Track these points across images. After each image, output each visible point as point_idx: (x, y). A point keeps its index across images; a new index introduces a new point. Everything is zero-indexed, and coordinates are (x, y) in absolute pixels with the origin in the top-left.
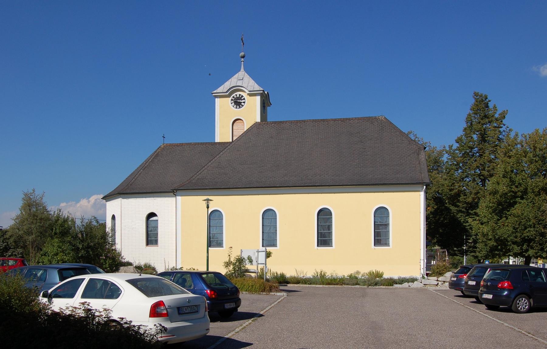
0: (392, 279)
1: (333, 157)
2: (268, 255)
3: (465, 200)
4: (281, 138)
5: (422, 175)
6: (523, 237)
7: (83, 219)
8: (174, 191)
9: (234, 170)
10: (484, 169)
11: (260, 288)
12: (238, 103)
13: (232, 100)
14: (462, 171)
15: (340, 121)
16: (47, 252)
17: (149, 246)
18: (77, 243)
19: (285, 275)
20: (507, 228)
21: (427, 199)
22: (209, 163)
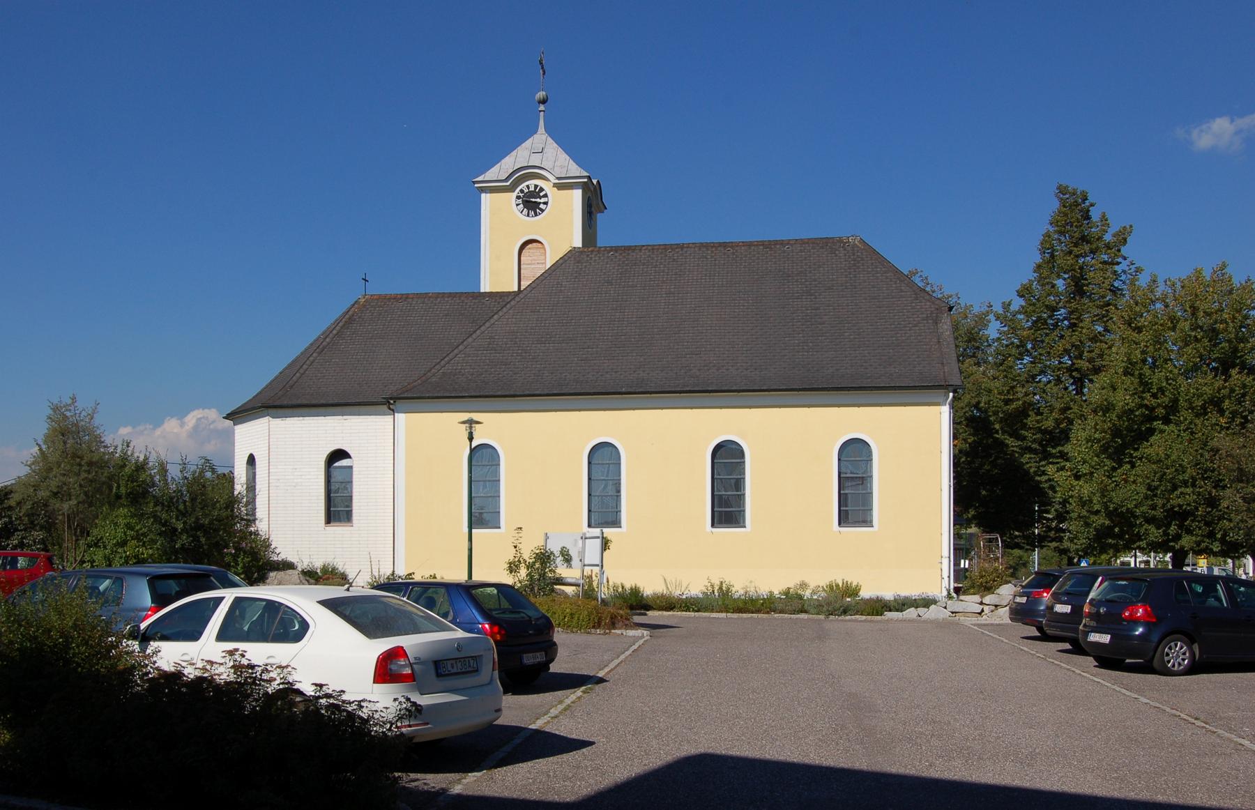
1: (746, 328)
2: (605, 544)
6: (1169, 507)
7: (185, 464)
8: (389, 402)
9: (524, 354)
10: (1080, 357)
11: (590, 620)
12: (532, 203)
13: (518, 197)
15: (761, 247)
16: (102, 538)
17: (332, 524)
18: (171, 518)
19: (642, 590)
20: (1133, 487)
21: (956, 423)
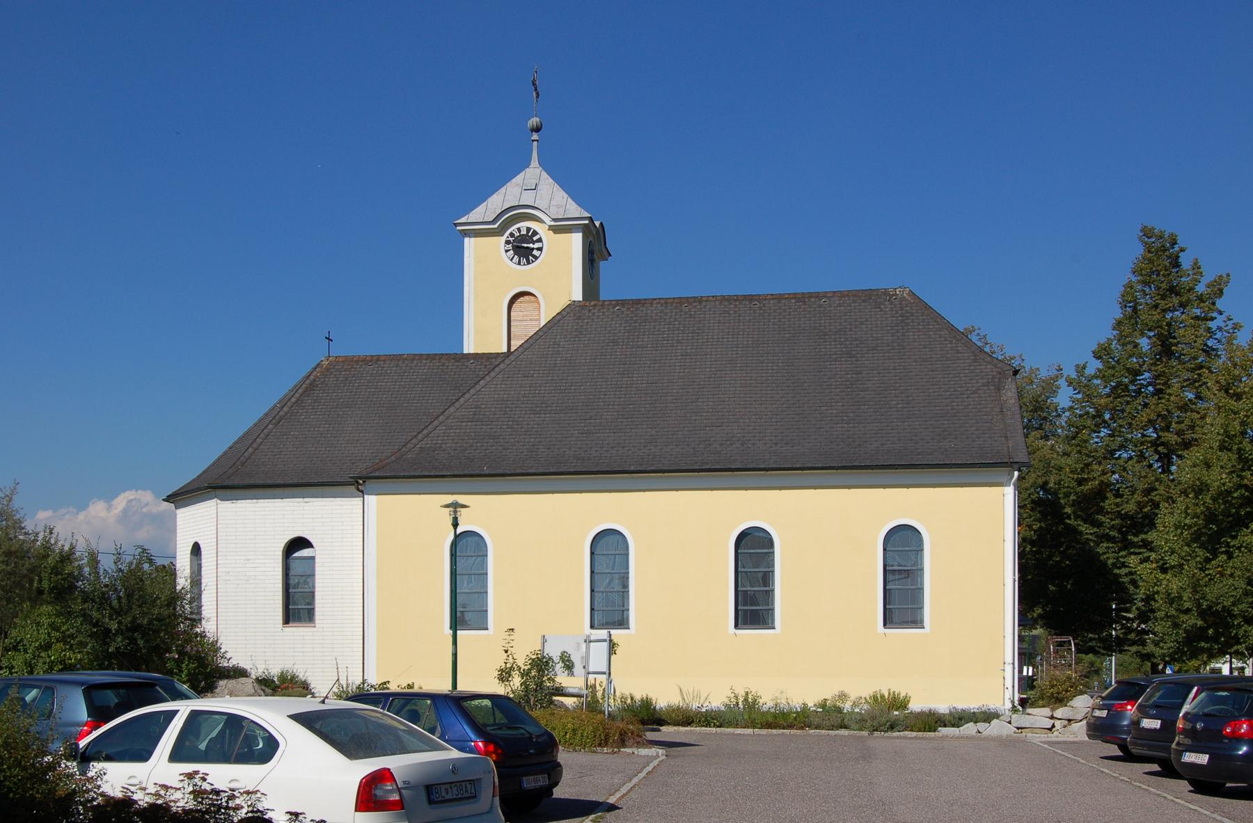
0: (934, 714)
3: (1117, 509)
4: (640, 343)
5: (1010, 442)
8: (357, 482)
11: (595, 736)
12: (524, 249)
13: (507, 242)
14: (1109, 432)
15: (793, 301)
16: (22, 640)
17: (290, 625)
20: (1231, 581)
22: (449, 407)
